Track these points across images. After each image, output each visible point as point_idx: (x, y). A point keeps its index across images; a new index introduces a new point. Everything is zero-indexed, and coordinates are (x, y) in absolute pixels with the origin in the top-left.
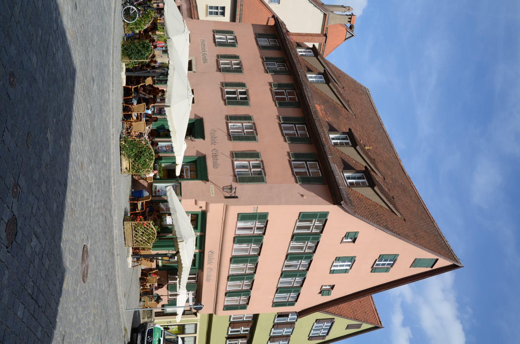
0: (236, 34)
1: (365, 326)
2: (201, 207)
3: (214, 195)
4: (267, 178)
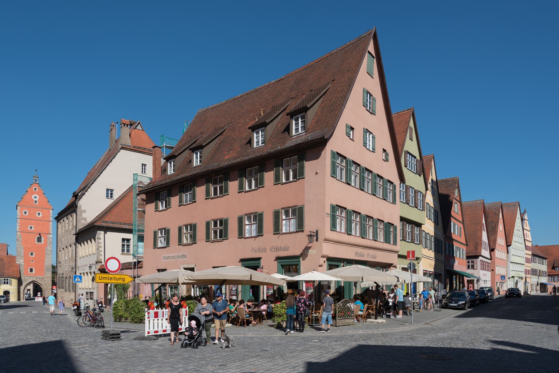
1: (412, 124)
2: (324, 262)
4: (299, 204)
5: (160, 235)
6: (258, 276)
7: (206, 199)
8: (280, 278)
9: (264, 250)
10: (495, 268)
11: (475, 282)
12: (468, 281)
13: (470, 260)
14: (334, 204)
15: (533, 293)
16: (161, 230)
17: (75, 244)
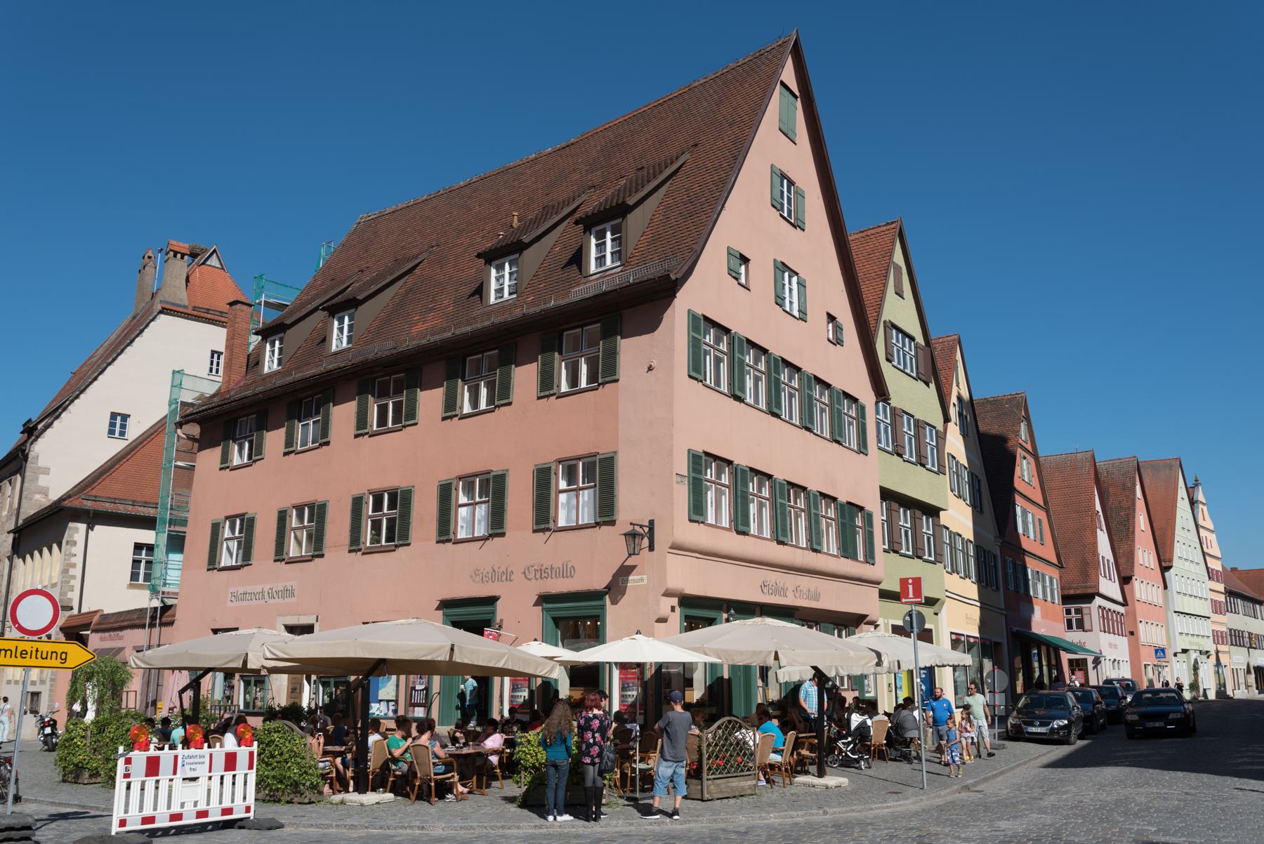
0: (219, 517)
1: (898, 257)
2: (673, 609)
3: (645, 577)
4: (604, 450)
5: (227, 533)
6: (477, 650)
7: (356, 436)
8: (546, 657)
9: (507, 576)
10: (1136, 627)
11: (1090, 665)
12: (1071, 661)
13: (1073, 607)
14: (699, 449)
15: (1240, 694)
16: (231, 518)
17: (10, 559)
